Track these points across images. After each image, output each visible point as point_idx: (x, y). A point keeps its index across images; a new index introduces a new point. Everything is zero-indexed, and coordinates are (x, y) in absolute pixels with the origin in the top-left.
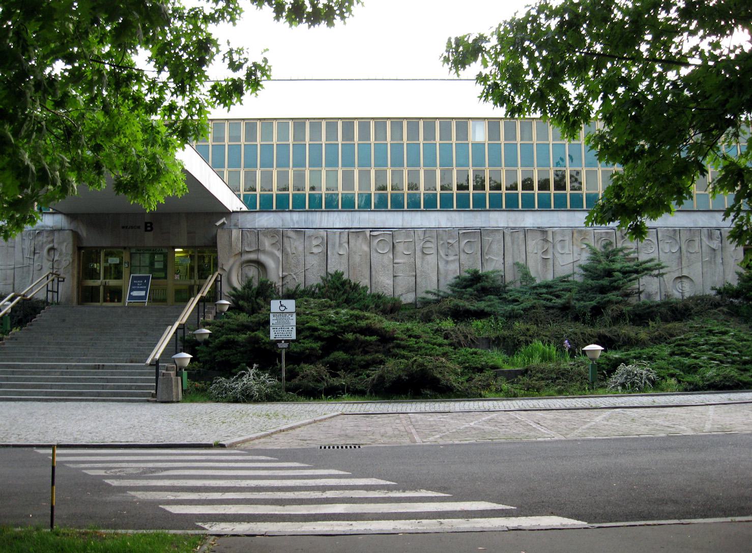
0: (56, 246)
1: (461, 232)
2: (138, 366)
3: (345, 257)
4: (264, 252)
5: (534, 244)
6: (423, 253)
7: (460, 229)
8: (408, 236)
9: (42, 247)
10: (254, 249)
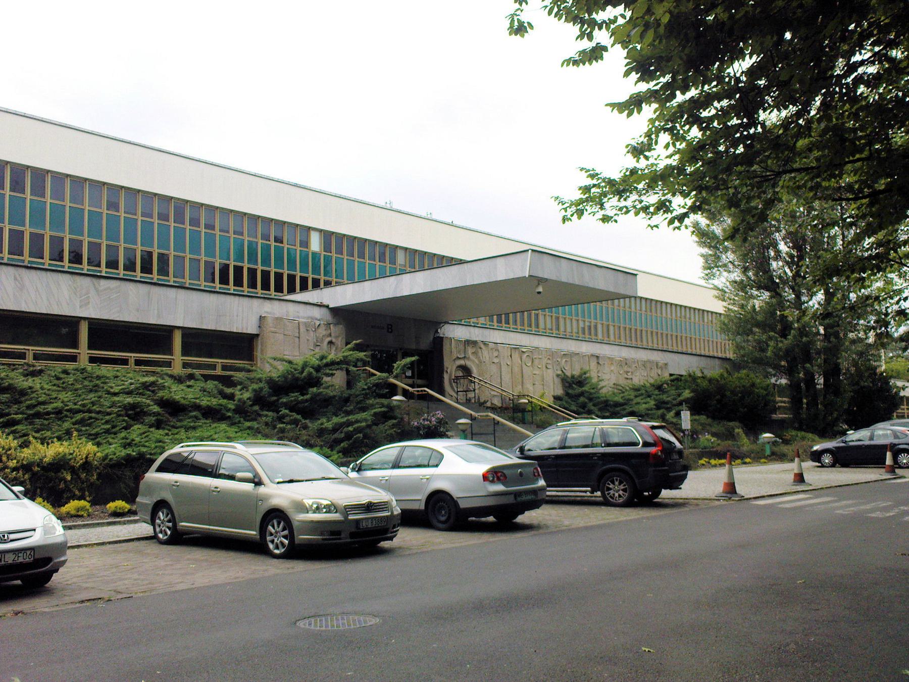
0: (334, 340)
4: (469, 359)
5: (593, 364)
9: (322, 341)
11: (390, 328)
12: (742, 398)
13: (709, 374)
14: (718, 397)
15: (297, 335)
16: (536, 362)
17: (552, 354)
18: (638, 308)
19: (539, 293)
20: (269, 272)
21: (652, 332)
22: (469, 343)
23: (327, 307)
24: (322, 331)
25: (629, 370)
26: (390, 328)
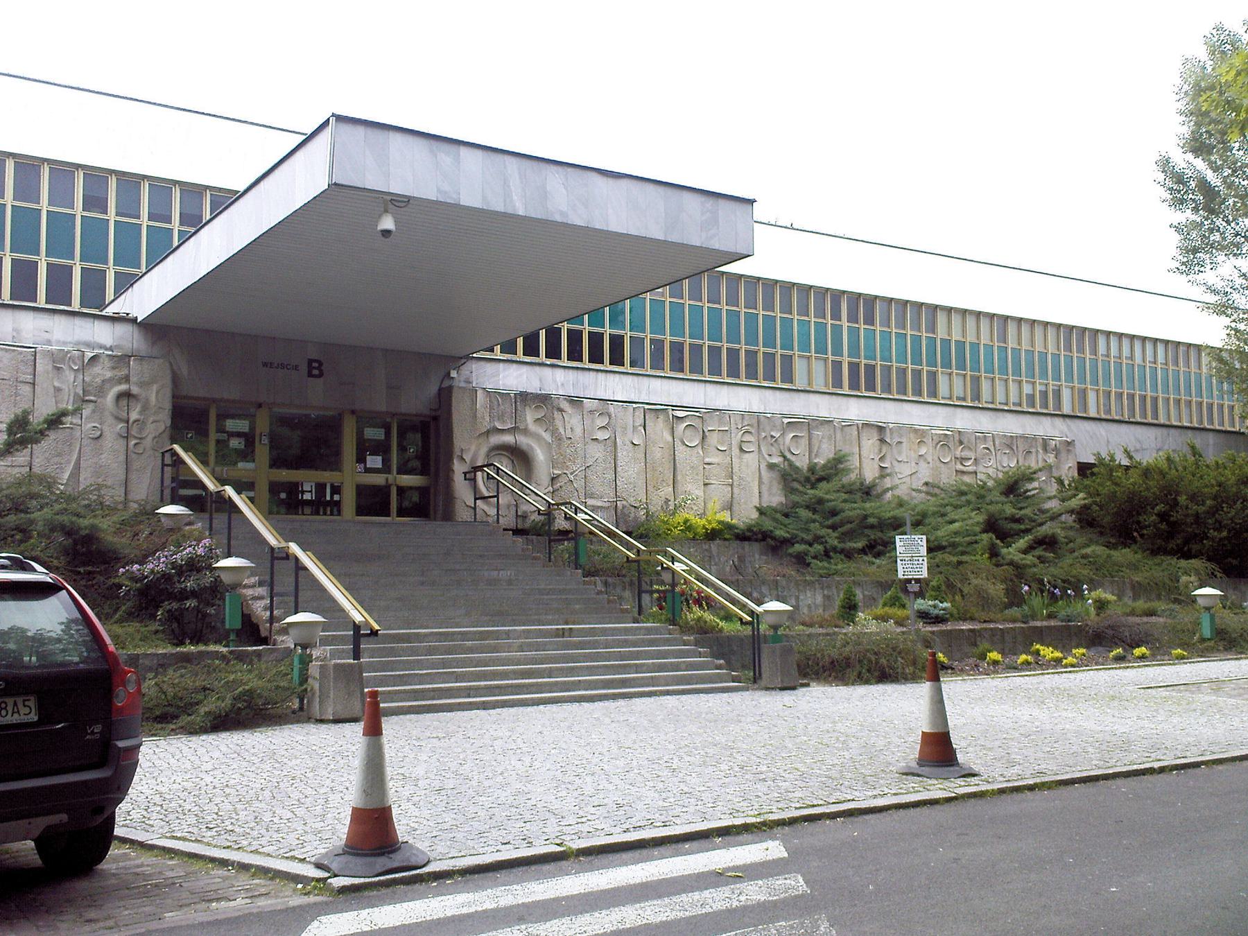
0: (135, 390)
1: (786, 421)
2: (615, 629)
3: (642, 449)
4: (526, 432)
5: (870, 442)
6: (741, 449)
7: (784, 416)
8: (721, 422)
9: (101, 391)
10: (509, 426)
11: (315, 368)
12: (1213, 512)
13: (1147, 458)
14: (1160, 508)
15: (29, 378)
16: (713, 439)
17: (757, 421)
18: (1149, 357)
19: (386, 233)
20: (858, 365)
21: (1178, 402)
22: (524, 398)
23: (134, 320)
24: (102, 371)
25: (966, 454)
26: (315, 368)
